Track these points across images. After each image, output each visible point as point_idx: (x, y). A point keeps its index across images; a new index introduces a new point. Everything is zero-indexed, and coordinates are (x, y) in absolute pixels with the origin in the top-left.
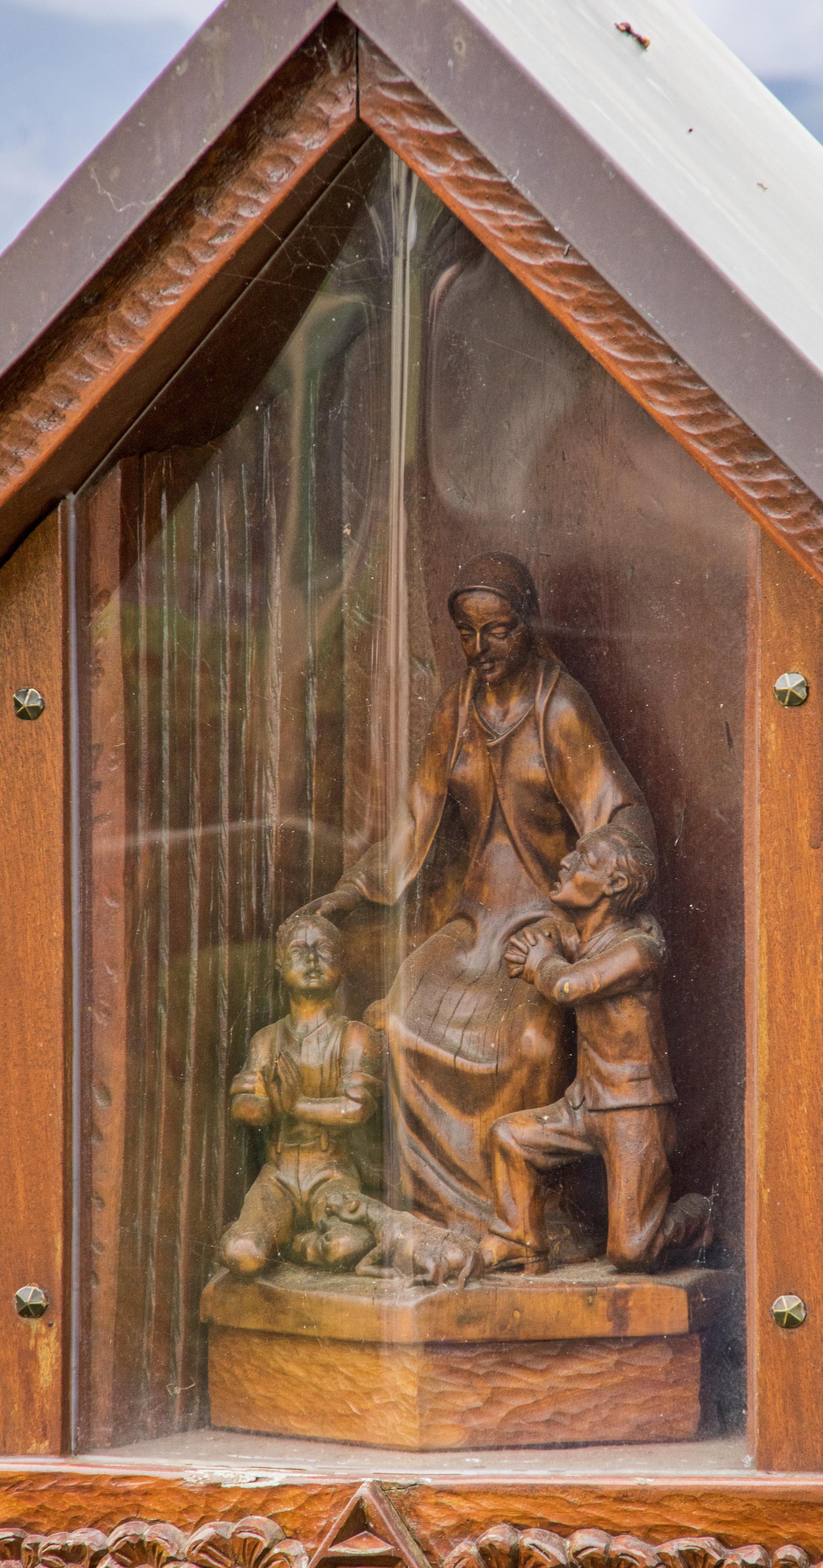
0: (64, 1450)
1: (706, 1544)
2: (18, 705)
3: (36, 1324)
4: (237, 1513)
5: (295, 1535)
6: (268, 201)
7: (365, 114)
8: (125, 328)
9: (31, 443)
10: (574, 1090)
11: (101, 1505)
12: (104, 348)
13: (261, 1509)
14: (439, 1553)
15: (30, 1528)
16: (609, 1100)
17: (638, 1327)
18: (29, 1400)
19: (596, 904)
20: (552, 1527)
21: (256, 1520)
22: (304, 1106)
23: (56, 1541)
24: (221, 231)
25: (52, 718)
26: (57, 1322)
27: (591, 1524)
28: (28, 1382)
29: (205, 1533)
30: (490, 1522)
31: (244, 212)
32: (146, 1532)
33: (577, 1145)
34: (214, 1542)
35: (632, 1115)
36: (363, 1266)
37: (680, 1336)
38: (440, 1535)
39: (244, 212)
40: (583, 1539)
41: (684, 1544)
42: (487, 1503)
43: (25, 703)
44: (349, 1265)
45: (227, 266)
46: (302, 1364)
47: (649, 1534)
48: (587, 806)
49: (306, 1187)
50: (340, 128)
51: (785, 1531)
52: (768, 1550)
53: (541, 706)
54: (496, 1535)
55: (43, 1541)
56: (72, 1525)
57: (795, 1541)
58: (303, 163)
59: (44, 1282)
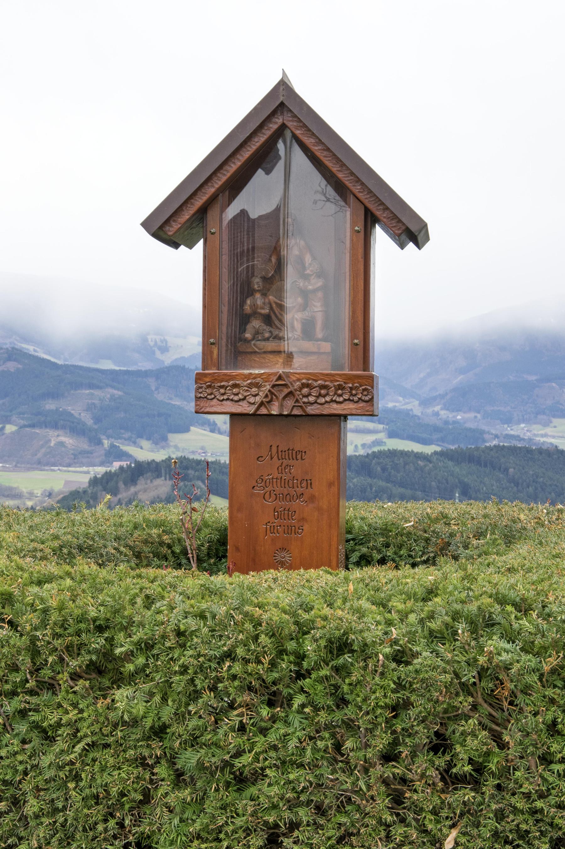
0: (218, 370)
1: (342, 383)
2: (210, 232)
3: (213, 346)
4: (254, 378)
5: (266, 382)
6: (266, 137)
7: (285, 122)
8: (238, 159)
9: (220, 180)
10: (308, 308)
11: (228, 378)
12: (234, 163)
13: (259, 377)
14: (294, 384)
15: (213, 383)
16: (316, 310)
17: (322, 351)
18: (212, 360)
19: (312, 275)
20: (314, 380)
21: (259, 379)
22: (259, 311)
23: (219, 384)
24: (257, 142)
25: (217, 235)
26: (217, 346)
27: (321, 379)
28: (212, 357)
29: (249, 381)
30: (303, 379)
31: (261, 139)
32: (237, 382)
33: (309, 319)
34: (250, 383)
35: (320, 313)
36: (271, 339)
37: (328, 353)
38: (294, 381)
39: (261, 139)
40: (319, 382)
41: (338, 383)
42: (303, 376)
43: (212, 231)
44: (268, 339)
45: (254, 152)
46: (258, 358)
47: (331, 381)
48: (306, 260)
49: (257, 326)
50: (280, 124)
51: (356, 381)
52: (353, 384)
53: (298, 241)
54: (304, 381)
55: (216, 385)
56: (222, 381)
57: (358, 383)
58: (273, 130)
59: (215, 339)
